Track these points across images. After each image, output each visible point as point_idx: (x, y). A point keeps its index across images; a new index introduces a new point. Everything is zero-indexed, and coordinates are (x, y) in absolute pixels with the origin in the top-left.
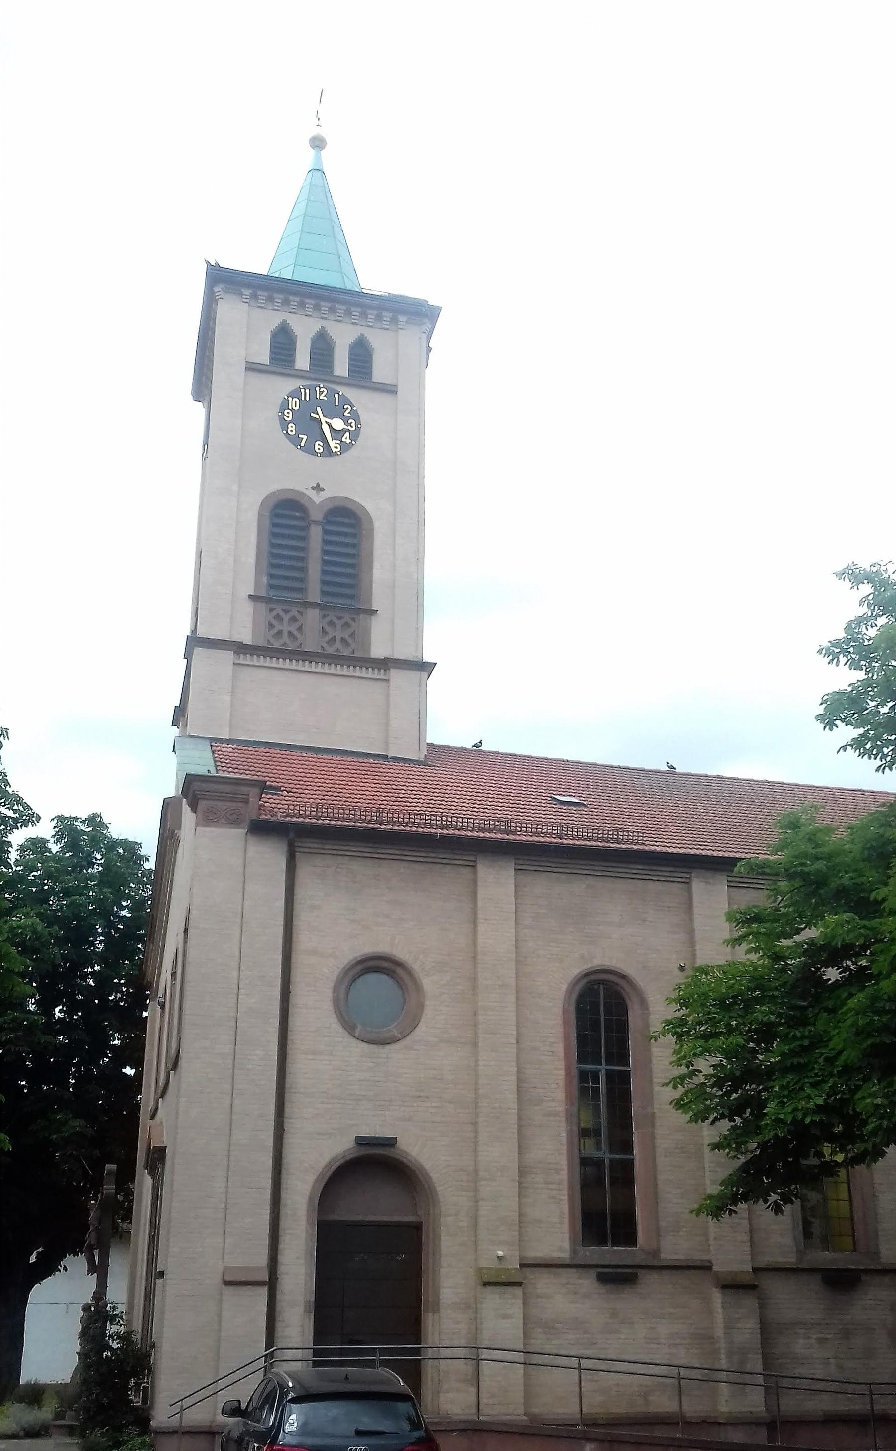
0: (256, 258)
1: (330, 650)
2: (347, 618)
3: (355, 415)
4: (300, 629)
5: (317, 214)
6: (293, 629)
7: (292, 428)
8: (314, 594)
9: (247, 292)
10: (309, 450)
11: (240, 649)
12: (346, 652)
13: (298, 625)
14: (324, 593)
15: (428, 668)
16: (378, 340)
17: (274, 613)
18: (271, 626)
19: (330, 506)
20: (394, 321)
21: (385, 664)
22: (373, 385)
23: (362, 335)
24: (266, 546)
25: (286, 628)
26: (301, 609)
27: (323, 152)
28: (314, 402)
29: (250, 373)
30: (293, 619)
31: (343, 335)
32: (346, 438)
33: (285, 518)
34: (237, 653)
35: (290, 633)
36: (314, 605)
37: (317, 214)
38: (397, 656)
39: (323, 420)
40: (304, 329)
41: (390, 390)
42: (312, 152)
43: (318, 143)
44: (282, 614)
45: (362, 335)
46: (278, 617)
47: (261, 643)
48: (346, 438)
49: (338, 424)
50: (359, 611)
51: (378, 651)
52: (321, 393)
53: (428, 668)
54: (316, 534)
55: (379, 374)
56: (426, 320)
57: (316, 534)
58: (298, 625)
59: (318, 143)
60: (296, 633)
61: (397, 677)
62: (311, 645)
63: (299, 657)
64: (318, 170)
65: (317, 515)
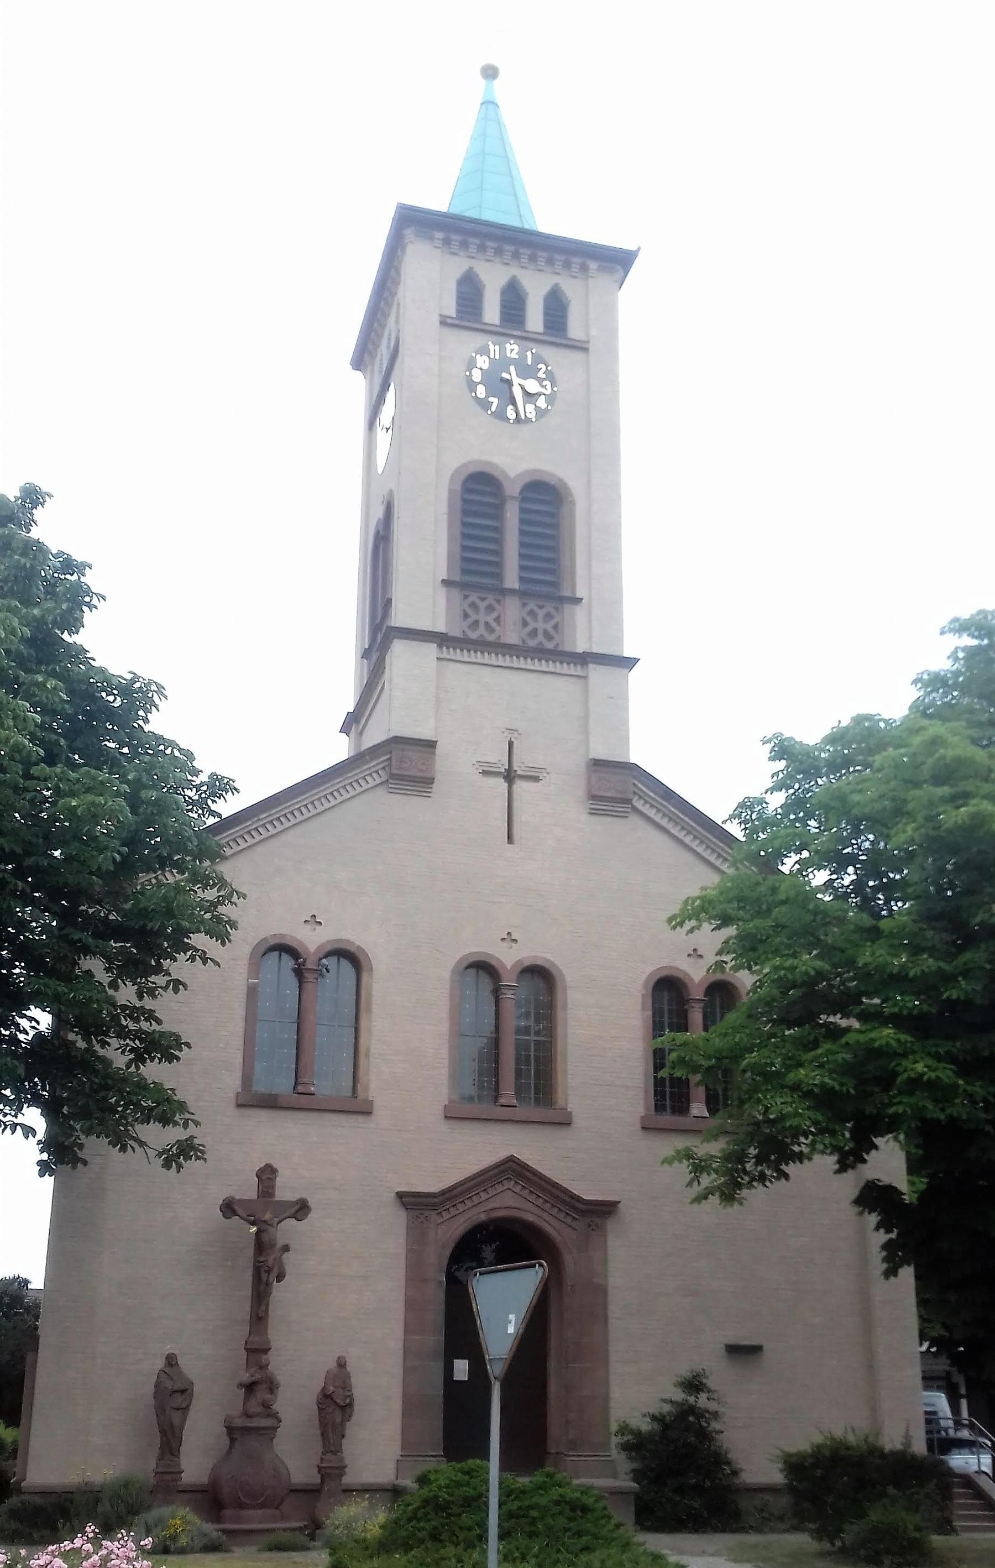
0: (437, 199)
1: (473, 635)
2: (491, 599)
3: (550, 376)
4: (497, 620)
5: (490, 151)
6: (549, 627)
7: (481, 391)
8: (511, 579)
9: (439, 235)
10: (500, 415)
11: (442, 640)
12: (491, 638)
13: (495, 615)
14: (521, 579)
15: (629, 663)
16: (571, 288)
17: (528, 608)
18: (466, 616)
19: (527, 480)
20: (584, 268)
21: (585, 659)
22: (569, 343)
23: (556, 285)
24: (458, 528)
25: (482, 618)
26: (499, 597)
27: (496, 82)
28: (504, 363)
29: (446, 330)
30: (548, 616)
31: (536, 288)
32: (541, 402)
33: (479, 494)
34: (440, 646)
35: (487, 624)
36: (512, 592)
37: (490, 151)
38: (595, 650)
39: (516, 381)
40: (493, 279)
41: (581, 347)
42: (482, 82)
43: (490, 73)
44: (478, 602)
45: (556, 285)
46: (473, 605)
47: (456, 633)
48: (541, 402)
49: (532, 386)
50: (562, 600)
51: (581, 646)
52: (512, 350)
53: (629, 663)
54: (512, 514)
55: (575, 331)
56: (619, 267)
57: (512, 514)
58: (495, 615)
59: (490, 73)
60: (494, 624)
61: (596, 673)
62: (512, 637)
63: (471, 646)
64: (489, 103)
65: (513, 490)
